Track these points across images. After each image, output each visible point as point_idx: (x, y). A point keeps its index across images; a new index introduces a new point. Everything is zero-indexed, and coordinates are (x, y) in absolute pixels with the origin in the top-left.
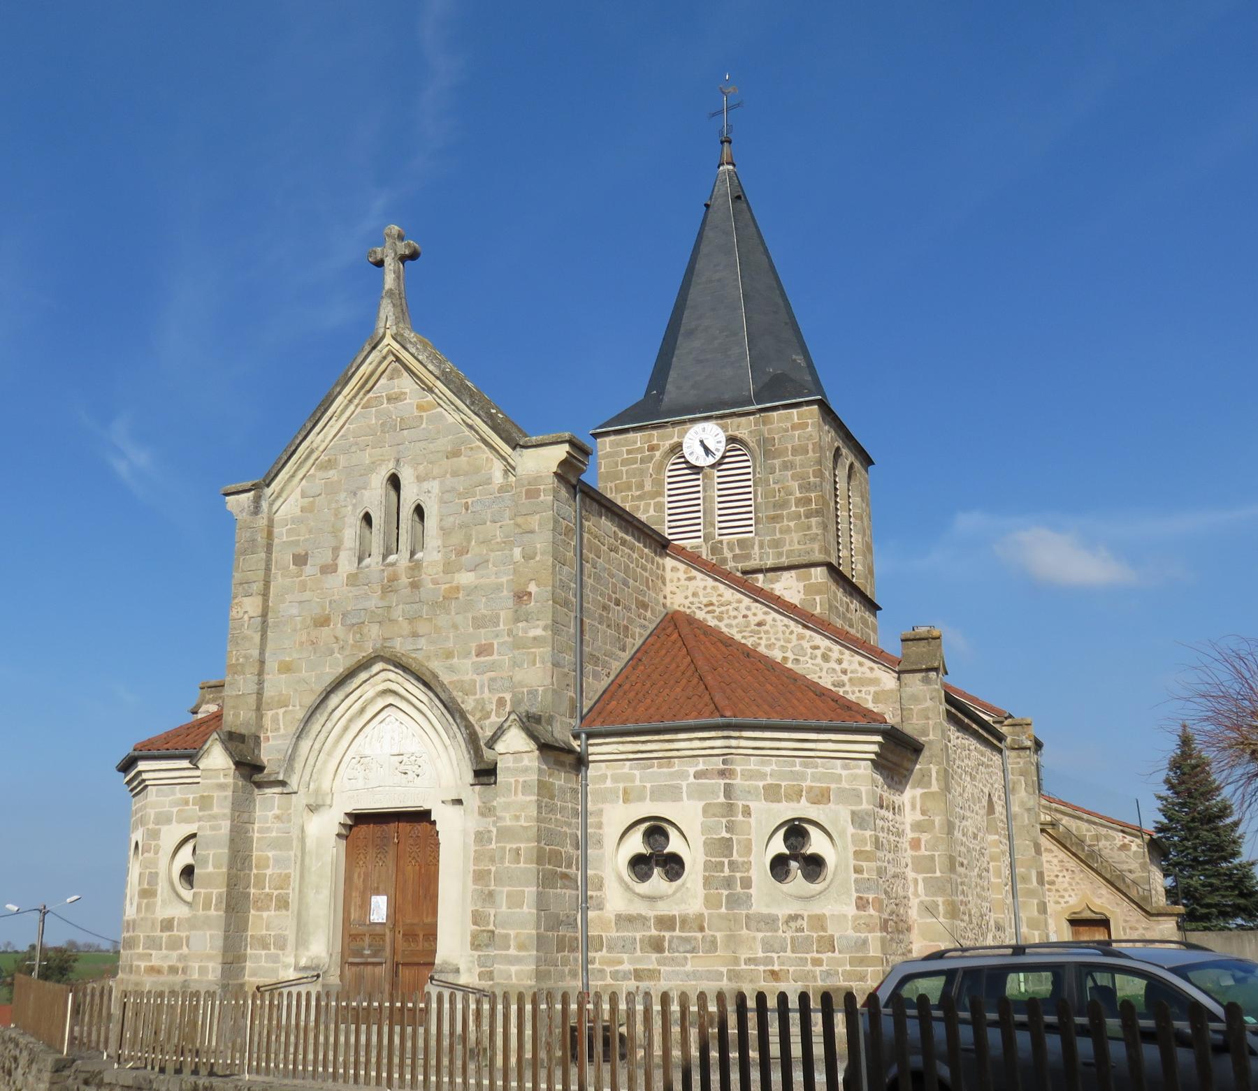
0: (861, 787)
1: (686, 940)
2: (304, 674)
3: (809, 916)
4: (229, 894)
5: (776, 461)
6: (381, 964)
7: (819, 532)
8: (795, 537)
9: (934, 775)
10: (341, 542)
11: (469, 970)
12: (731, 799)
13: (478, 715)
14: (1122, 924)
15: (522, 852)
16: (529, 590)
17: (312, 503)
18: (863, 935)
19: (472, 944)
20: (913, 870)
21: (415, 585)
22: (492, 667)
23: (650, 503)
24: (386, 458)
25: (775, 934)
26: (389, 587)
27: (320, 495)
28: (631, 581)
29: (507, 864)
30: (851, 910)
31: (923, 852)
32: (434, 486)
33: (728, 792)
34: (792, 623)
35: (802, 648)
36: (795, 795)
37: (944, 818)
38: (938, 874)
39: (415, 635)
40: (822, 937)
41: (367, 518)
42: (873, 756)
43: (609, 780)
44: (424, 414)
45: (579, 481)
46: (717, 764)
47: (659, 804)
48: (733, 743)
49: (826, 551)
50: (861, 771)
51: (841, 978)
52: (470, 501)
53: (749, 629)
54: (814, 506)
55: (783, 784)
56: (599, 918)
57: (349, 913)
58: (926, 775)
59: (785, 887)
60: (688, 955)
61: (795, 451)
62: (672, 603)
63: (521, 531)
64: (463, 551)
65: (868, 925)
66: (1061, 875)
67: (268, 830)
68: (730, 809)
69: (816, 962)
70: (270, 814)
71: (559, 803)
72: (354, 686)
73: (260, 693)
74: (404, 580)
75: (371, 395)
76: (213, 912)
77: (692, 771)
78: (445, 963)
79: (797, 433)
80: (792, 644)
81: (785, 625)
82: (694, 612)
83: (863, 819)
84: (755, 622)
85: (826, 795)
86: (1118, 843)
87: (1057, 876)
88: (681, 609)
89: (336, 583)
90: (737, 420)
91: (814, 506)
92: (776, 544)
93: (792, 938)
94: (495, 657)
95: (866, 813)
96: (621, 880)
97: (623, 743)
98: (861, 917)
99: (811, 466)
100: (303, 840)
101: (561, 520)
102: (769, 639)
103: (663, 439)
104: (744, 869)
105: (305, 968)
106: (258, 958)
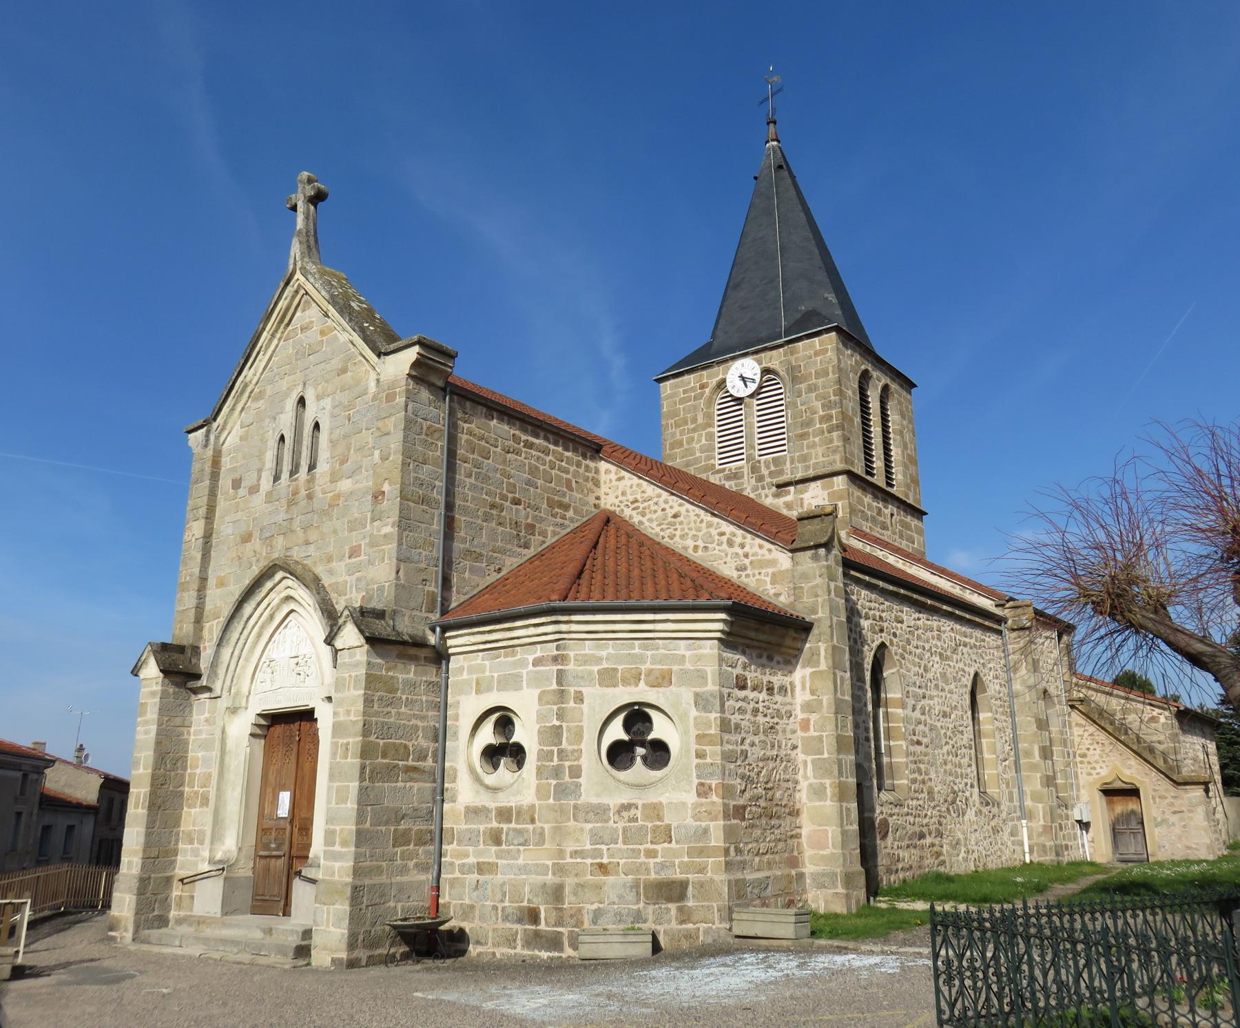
1: (520, 832)
3: (644, 805)
8: (820, 450)
9: (823, 653)
10: (263, 464)
14: (1151, 793)
15: (350, 747)
18: (704, 824)
20: (803, 752)
21: (310, 497)
25: (605, 825)
29: (338, 760)
30: (691, 798)
32: (327, 403)
34: (702, 512)
36: (634, 678)
37: (832, 696)
38: (826, 755)
39: (307, 543)
40: (658, 827)
41: (282, 438)
42: (718, 635)
43: (465, 672)
44: (324, 338)
45: (447, 383)
46: (551, 650)
47: (504, 693)
48: (564, 627)
49: (846, 460)
50: (707, 651)
51: (678, 870)
52: (351, 412)
54: (835, 422)
55: (620, 668)
58: (815, 653)
59: (623, 775)
60: (521, 848)
61: (818, 375)
63: (380, 434)
64: (343, 461)
65: (710, 813)
66: (1092, 747)
68: (561, 695)
70: (202, 717)
71: (404, 697)
72: (263, 594)
75: (290, 328)
77: (531, 658)
79: (818, 359)
81: (697, 515)
82: (622, 510)
83: (707, 701)
85: (667, 677)
86: (1146, 717)
87: (1088, 749)
88: (612, 509)
89: (258, 500)
90: (769, 353)
91: (835, 422)
92: (804, 458)
93: (625, 830)
95: (712, 695)
96: (472, 770)
97: (473, 634)
98: (702, 805)
99: (831, 387)
102: (683, 529)
103: (709, 377)
104: (573, 758)
105: (220, 862)
106: (185, 851)
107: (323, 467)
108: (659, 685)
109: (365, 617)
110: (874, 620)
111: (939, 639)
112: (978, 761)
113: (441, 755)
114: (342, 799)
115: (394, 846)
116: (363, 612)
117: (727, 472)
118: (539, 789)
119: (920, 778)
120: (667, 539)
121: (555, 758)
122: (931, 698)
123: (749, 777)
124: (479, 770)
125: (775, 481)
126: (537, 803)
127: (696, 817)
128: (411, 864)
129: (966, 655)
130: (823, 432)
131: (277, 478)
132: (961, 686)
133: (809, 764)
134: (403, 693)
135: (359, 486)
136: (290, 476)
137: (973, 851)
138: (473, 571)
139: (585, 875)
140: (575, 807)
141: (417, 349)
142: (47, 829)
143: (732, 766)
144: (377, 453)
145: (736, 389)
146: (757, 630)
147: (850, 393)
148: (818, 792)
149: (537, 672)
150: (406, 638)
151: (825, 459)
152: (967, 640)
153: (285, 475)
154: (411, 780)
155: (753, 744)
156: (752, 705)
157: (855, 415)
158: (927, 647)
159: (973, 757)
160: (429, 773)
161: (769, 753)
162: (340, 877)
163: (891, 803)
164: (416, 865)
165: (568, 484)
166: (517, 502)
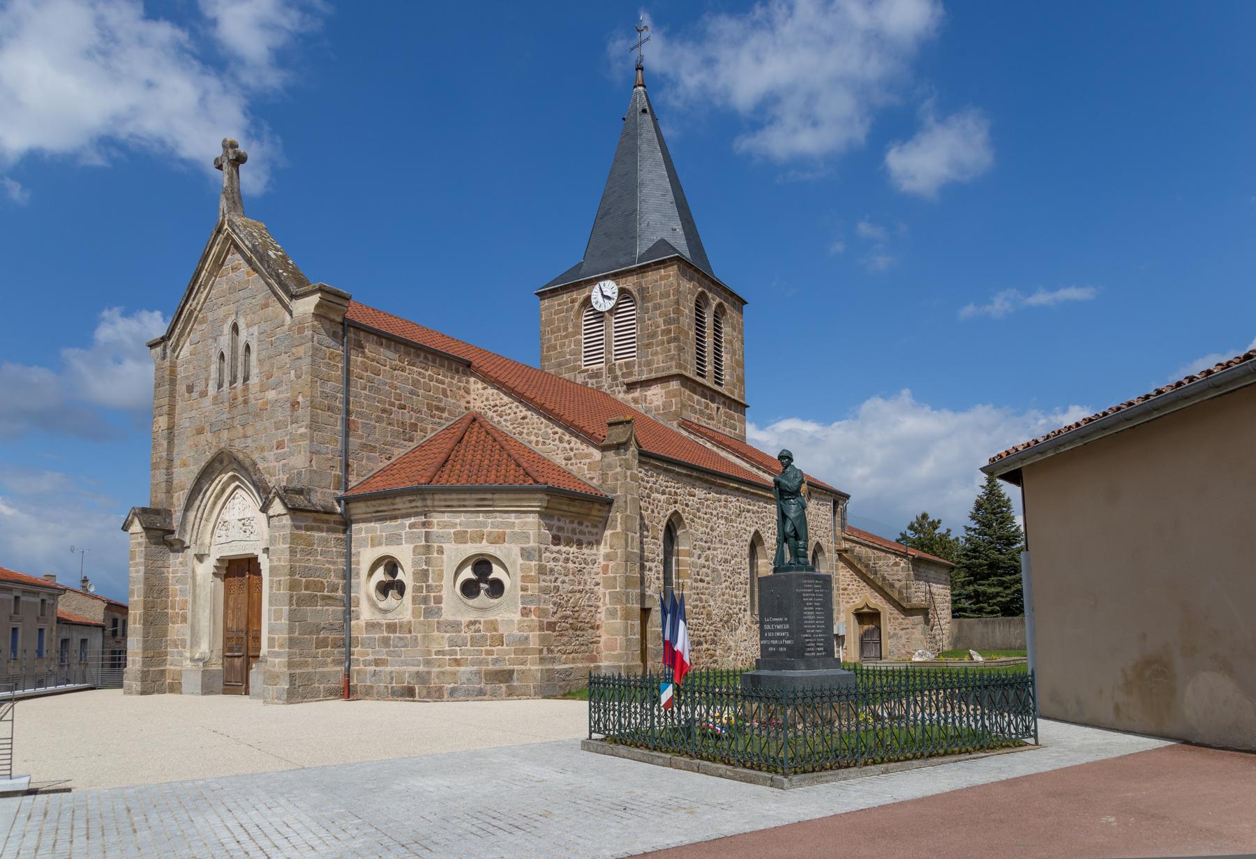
0: (529, 531)
1: (401, 639)
3: (484, 621)
5: (649, 304)
7: (676, 353)
8: (660, 357)
9: (619, 520)
12: (428, 542)
14: (888, 615)
15: (282, 582)
21: (246, 402)
27: (199, 342)
30: (517, 617)
32: (255, 330)
38: (618, 589)
39: (245, 437)
41: (222, 356)
43: (363, 532)
44: (250, 278)
47: (390, 547)
53: (517, 422)
54: (673, 335)
55: (469, 530)
56: (357, 625)
57: (227, 624)
59: (471, 602)
61: (662, 296)
62: (474, 407)
63: (294, 358)
66: (851, 584)
68: (428, 549)
69: (489, 653)
71: (319, 549)
72: (335, 301)
76: (137, 626)
82: (486, 412)
84: (521, 417)
87: (849, 585)
89: (207, 402)
91: (673, 335)
92: (649, 364)
93: (472, 638)
96: (369, 598)
101: (323, 348)
103: (580, 296)
107: (254, 380)
108: (496, 543)
109: (286, 494)
110: (670, 494)
111: (725, 507)
113: (348, 588)
114: (278, 618)
115: (316, 648)
116: (286, 490)
118: (413, 612)
120: (517, 435)
121: (424, 591)
122: (715, 549)
123: (560, 603)
124: (375, 599)
125: (626, 380)
126: (413, 620)
127: (520, 629)
128: (329, 660)
129: (749, 519)
130: (664, 343)
131: (220, 386)
132: (742, 541)
134: (318, 546)
135: (281, 396)
136: (230, 385)
137: (742, 654)
139: (445, 666)
140: (438, 623)
141: (319, 295)
142: (65, 642)
143: (547, 596)
144: (293, 372)
146: (568, 505)
147: (687, 311)
148: (612, 614)
149: (412, 533)
150: (319, 508)
151: (664, 365)
153: (226, 385)
154: (327, 605)
155: (563, 582)
156: (564, 555)
159: (748, 592)
160: (340, 600)
161: (576, 588)
164: (333, 661)
165: (444, 393)
166: (403, 407)
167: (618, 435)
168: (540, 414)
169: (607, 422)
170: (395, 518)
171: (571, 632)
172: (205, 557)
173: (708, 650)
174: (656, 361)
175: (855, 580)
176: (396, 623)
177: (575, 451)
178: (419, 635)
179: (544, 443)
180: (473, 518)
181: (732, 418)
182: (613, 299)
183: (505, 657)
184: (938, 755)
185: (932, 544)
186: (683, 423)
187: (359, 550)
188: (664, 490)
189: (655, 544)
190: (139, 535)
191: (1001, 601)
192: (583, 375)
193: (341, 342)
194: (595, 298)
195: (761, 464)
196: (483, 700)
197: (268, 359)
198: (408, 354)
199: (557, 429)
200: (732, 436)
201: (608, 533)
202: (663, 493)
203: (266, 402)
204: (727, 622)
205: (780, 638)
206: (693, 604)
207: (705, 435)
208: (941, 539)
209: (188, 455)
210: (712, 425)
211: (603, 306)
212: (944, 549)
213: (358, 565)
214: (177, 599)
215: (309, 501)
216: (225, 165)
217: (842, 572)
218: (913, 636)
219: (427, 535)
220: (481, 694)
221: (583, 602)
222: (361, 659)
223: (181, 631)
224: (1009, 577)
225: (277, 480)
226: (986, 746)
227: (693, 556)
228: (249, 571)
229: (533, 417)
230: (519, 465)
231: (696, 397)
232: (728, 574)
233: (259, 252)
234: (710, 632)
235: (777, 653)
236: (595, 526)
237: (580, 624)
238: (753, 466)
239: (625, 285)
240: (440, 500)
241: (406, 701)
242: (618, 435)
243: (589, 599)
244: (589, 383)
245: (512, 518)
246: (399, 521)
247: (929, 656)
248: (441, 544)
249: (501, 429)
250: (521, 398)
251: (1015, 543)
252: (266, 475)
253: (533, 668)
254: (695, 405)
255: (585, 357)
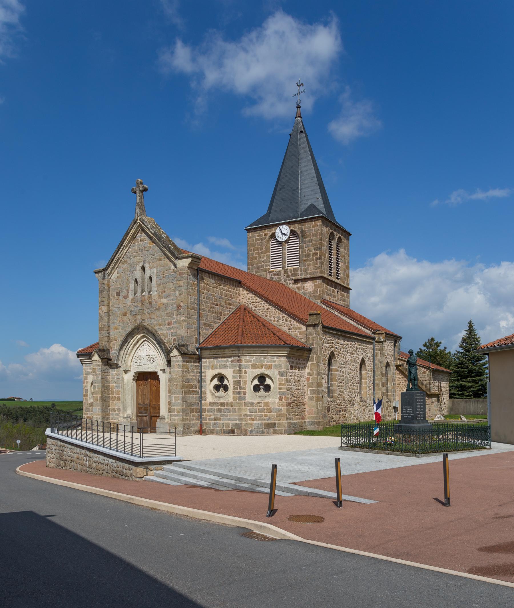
2: (121, 331)
4: (102, 397)
5: (306, 239)
6: (147, 416)
8: (312, 267)
9: (315, 358)
11: (168, 418)
13: (168, 344)
15: (178, 385)
16: (181, 305)
17: (121, 275)
19: (168, 411)
21: (150, 303)
22: (172, 329)
23: (264, 255)
24: (141, 261)
26: (143, 303)
28: (223, 297)
30: (277, 400)
31: (310, 382)
33: (240, 366)
35: (280, 317)
38: (314, 388)
40: (268, 408)
41: (136, 281)
43: (208, 363)
44: (151, 246)
54: (318, 256)
55: (257, 363)
56: (205, 403)
57: (138, 401)
61: (313, 236)
66: (402, 382)
67: (114, 378)
68: (240, 371)
69: (266, 415)
70: (114, 373)
71: (191, 370)
73: (109, 337)
74: (147, 301)
76: (98, 402)
78: (162, 416)
79: (314, 228)
80: (277, 316)
87: (401, 382)
89: (128, 301)
91: (318, 256)
92: (306, 270)
93: (259, 409)
94: (173, 326)
96: (211, 392)
100: (123, 380)
101: (191, 282)
103: (270, 232)
106: (113, 414)
108: (268, 369)
110: (330, 344)
112: (361, 387)
113: (201, 387)
117: (274, 272)
118: (233, 398)
119: (341, 394)
120: (264, 317)
121: (239, 389)
122: (346, 368)
124: (213, 392)
125: (294, 278)
127: (278, 406)
128: (195, 418)
132: (357, 363)
133: (309, 391)
135: (169, 302)
137: (356, 416)
138: (206, 329)
139: (248, 421)
140: (245, 403)
141: (191, 259)
143: (288, 392)
145: (279, 238)
146: (296, 352)
147: (325, 243)
148: (311, 399)
151: (314, 271)
152: (360, 347)
154: (194, 394)
155: (294, 385)
156: (294, 374)
157: (326, 252)
158: (346, 350)
159: (359, 387)
161: (298, 388)
162: (178, 421)
163: (331, 402)
164: (196, 418)
166: (217, 305)
167: (313, 320)
168: (276, 308)
169: (309, 313)
170: (224, 357)
171: (296, 407)
172: (128, 371)
173: (343, 414)
174: (309, 269)
175: (404, 380)
176: (225, 403)
177: (293, 326)
178: (236, 408)
179: (278, 321)
180: (258, 358)
181: (343, 296)
182: (287, 235)
183: (272, 417)
184: (461, 450)
185: (436, 355)
186: (323, 301)
187: (205, 370)
188: (328, 342)
189: (325, 367)
190: (98, 361)
191: (473, 390)
192: (271, 273)
193: (196, 278)
194: (277, 234)
195: (363, 324)
196: (263, 435)
197: (162, 284)
198: (219, 280)
199: (284, 315)
200: (343, 305)
201: (309, 363)
202: (328, 343)
203: (162, 304)
204: (350, 401)
205: (409, 413)
206: (338, 393)
207: (335, 308)
208: (441, 353)
209: (118, 325)
210: (335, 300)
211: (282, 238)
212: (442, 358)
213: (206, 377)
214: (114, 390)
215: (187, 350)
216: (138, 192)
217: (398, 376)
218: (432, 408)
219: (240, 365)
220: (262, 433)
221: (300, 394)
222: (207, 418)
223: (117, 404)
224: (478, 378)
225: (169, 340)
226: (475, 448)
227: (338, 372)
228: (150, 378)
229: (272, 309)
230: (274, 334)
231: (328, 287)
232: (351, 379)
233: (158, 236)
234: (344, 406)
235: (407, 418)
236: (304, 360)
237: (299, 403)
238: (358, 324)
239: (293, 229)
240: (246, 351)
241: (231, 435)
242: (313, 320)
243: (302, 392)
244: (274, 278)
245: (275, 358)
246: (226, 359)
247: (442, 418)
248: (246, 370)
249: (256, 313)
250: (266, 300)
251: (482, 360)
252: (162, 337)
253: (284, 422)
254: (328, 291)
255: (271, 264)
